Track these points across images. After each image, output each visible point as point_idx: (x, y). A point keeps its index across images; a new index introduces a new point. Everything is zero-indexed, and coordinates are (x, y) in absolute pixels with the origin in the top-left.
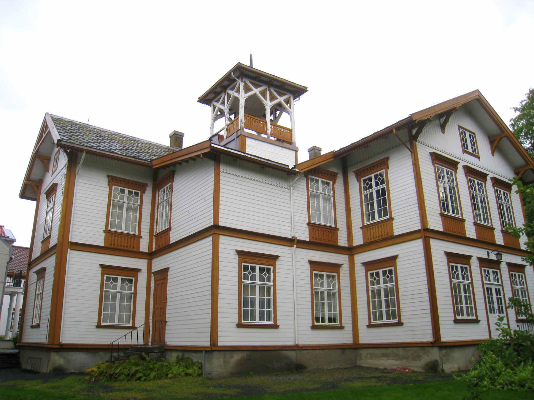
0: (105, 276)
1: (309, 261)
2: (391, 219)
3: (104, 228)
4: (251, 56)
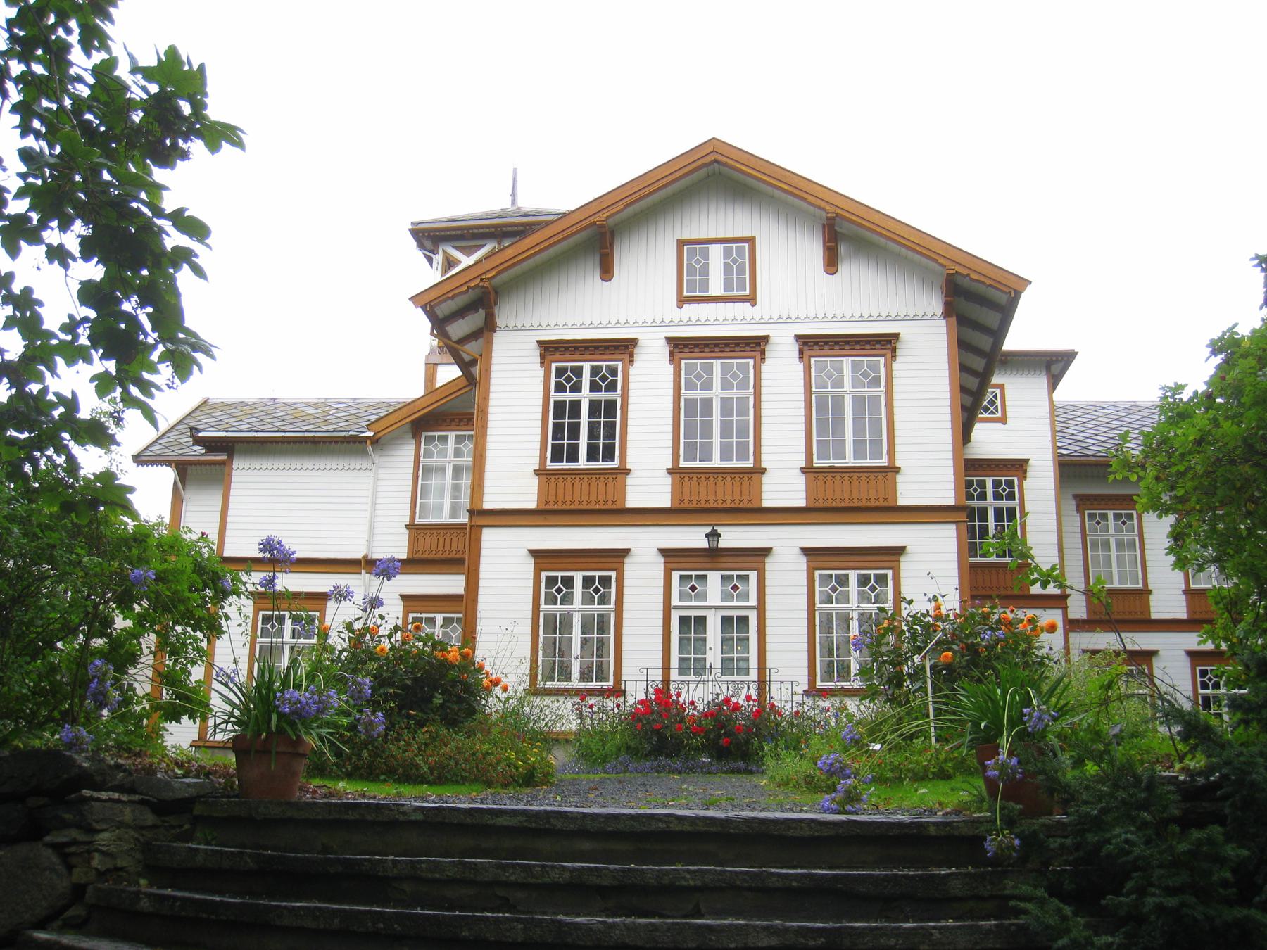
0: (544, 574)
1: (530, 551)
2: (627, 472)
3: (1183, 587)
4: (515, 171)
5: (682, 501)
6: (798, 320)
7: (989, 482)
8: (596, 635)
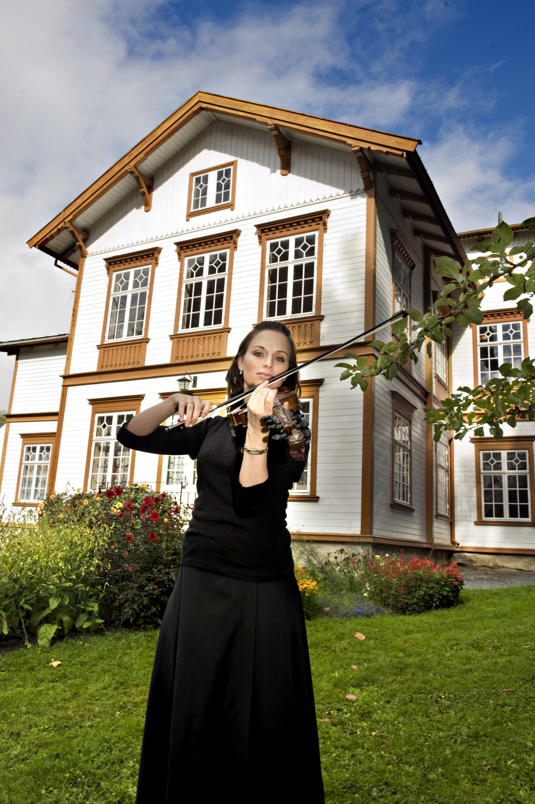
2: (146, 340)
5: (102, 367)
6: (255, 216)
7: (499, 327)
8: (518, 489)
